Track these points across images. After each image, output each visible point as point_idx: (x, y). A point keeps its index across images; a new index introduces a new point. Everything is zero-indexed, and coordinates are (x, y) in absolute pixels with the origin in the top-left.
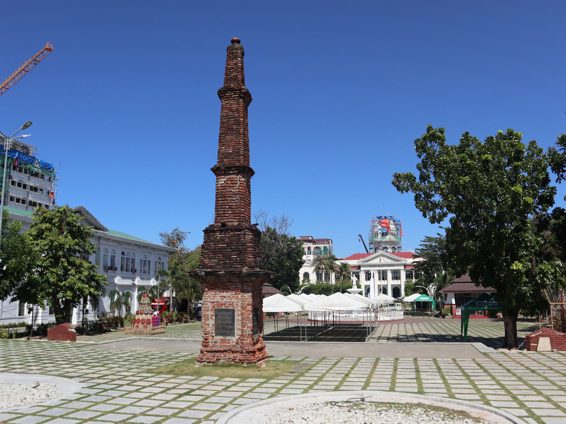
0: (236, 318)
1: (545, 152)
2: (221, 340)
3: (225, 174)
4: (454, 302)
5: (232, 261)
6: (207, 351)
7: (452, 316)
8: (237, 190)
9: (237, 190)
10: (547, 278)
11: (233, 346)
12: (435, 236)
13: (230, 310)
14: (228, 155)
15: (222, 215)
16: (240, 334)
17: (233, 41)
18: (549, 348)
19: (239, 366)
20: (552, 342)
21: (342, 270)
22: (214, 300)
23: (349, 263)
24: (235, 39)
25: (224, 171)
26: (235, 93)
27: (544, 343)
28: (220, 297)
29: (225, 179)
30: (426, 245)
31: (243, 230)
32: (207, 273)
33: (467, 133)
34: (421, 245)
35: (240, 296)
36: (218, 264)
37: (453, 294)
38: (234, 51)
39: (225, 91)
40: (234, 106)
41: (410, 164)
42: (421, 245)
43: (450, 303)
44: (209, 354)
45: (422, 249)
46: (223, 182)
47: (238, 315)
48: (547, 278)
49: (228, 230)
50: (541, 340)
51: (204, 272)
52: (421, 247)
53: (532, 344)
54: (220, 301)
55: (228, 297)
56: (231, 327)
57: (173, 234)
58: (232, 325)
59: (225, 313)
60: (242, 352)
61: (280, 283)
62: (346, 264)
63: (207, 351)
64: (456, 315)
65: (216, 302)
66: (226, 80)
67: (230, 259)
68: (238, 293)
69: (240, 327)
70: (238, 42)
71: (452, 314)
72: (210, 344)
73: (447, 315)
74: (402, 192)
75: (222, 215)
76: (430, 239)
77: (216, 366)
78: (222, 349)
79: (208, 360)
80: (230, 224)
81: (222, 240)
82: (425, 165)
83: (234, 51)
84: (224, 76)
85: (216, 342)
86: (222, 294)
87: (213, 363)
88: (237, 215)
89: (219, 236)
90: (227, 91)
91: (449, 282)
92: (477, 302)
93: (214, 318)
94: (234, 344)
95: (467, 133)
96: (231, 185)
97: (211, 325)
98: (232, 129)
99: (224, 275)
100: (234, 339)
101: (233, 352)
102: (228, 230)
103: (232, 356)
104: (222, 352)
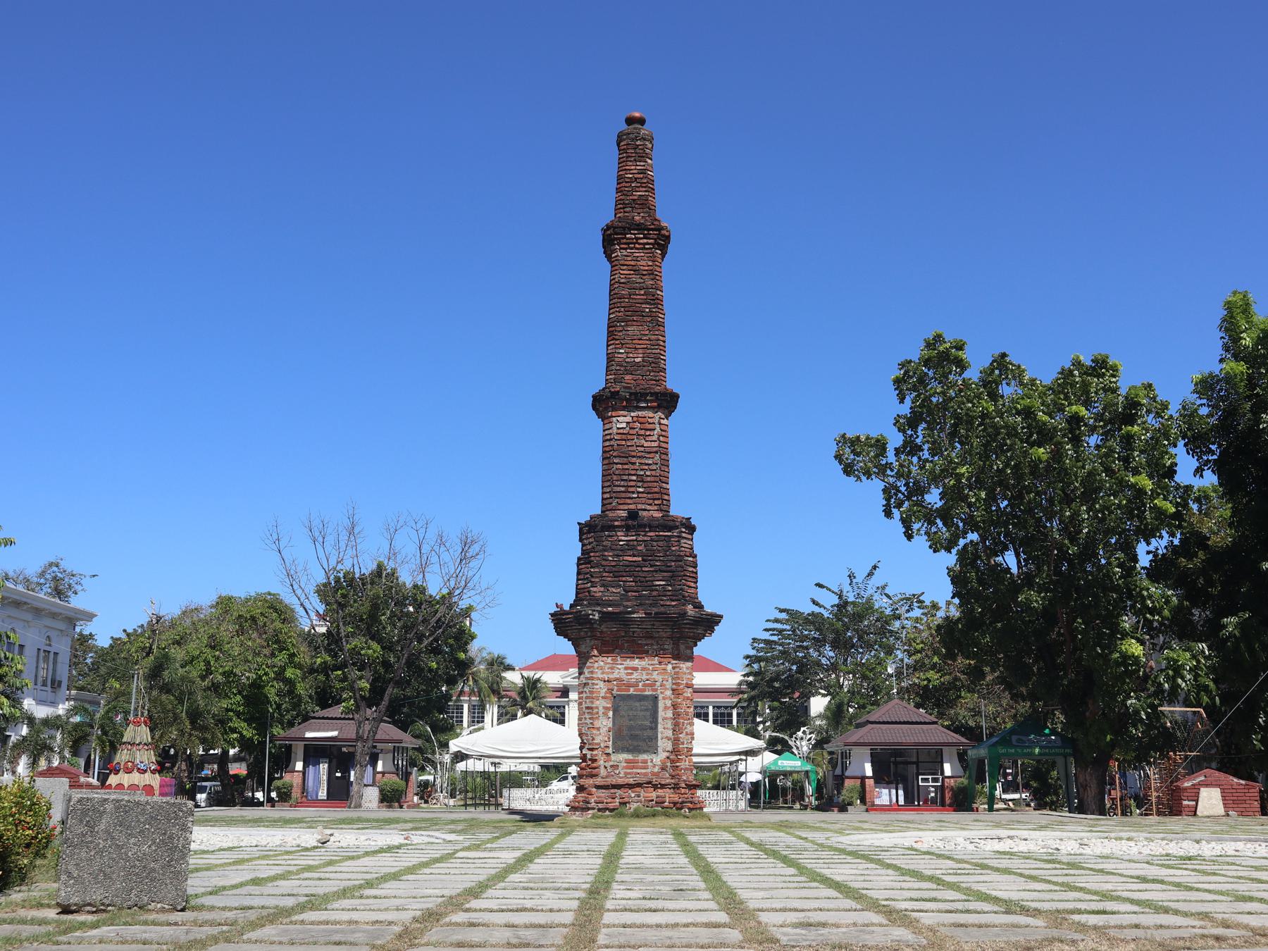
0: (661, 714)
1: (1173, 410)
2: (627, 761)
3: (628, 408)
4: (868, 770)
5: (655, 593)
6: (598, 787)
7: (864, 808)
8: (656, 444)
9: (654, 444)
10: (1183, 678)
11: (653, 774)
12: (808, 608)
13: (647, 696)
14: (631, 368)
15: (623, 495)
16: (670, 748)
17: (630, 121)
18: (1220, 810)
19: (674, 816)
20: (1224, 798)
21: (524, 698)
22: (611, 676)
23: (544, 679)
24: (637, 115)
25: (627, 400)
26: (634, 233)
27: (1210, 800)
28: (626, 668)
29: (629, 419)
30: (781, 631)
31: (677, 527)
32: (605, 617)
33: (1004, 355)
34: (766, 630)
35: (669, 667)
36: (625, 597)
37: (867, 751)
38: (633, 143)
39: (624, 228)
40: (643, 263)
41: (881, 415)
42: (766, 630)
43: (859, 774)
44: (602, 794)
45: (767, 642)
46: (624, 425)
47: (666, 708)
48: (1183, 678)
49: (645, 526)
50: (1204, 792)
51: (600, 612)
52: (766, 636)
53: (1185, 803)
54: (625, 677)
55: (644, 669)
56: (649, 733)
57: (42, 574)
58: (651, 728)
59: (637, 704)
60: (676, 787)
61: (407, 716)
62: (538, 680)
63: (598, 787)
64: (873, 805)
65: (616, 679)
66: (621, 205)
67: (651, 588)
68: (666, 660)
69: (670, 733)
70: (642, 121)
71: (863, 801)
72: (603, 772)
73: (850, 804)
74: (859, 478)
75: (623, 495)
76: (793, 615)
77: (622, 815)
78: (631, 781)
79: (600, 806)
80: (645, 513)
81: (630, 547)
82: (912, 422)
83: (633, 143)
84: (612, 196)
85: (615, 767)
86: (629, 663)
87: (611, 810)
88: (657, 496)
89: (623, 538)
90: (630, 229)
91: (851, 723)
92: (1014, 738)
93: (611, 714)
94: (656, 770)
95: (1004, 355)
96: (642, 432)
97: (604, 730)
98: (640, 313)
99: (642, 620)
100: (658, 759)
101: (655, 787)
102: (645, 526)
103: (653, 795)
104: (631, 786)
